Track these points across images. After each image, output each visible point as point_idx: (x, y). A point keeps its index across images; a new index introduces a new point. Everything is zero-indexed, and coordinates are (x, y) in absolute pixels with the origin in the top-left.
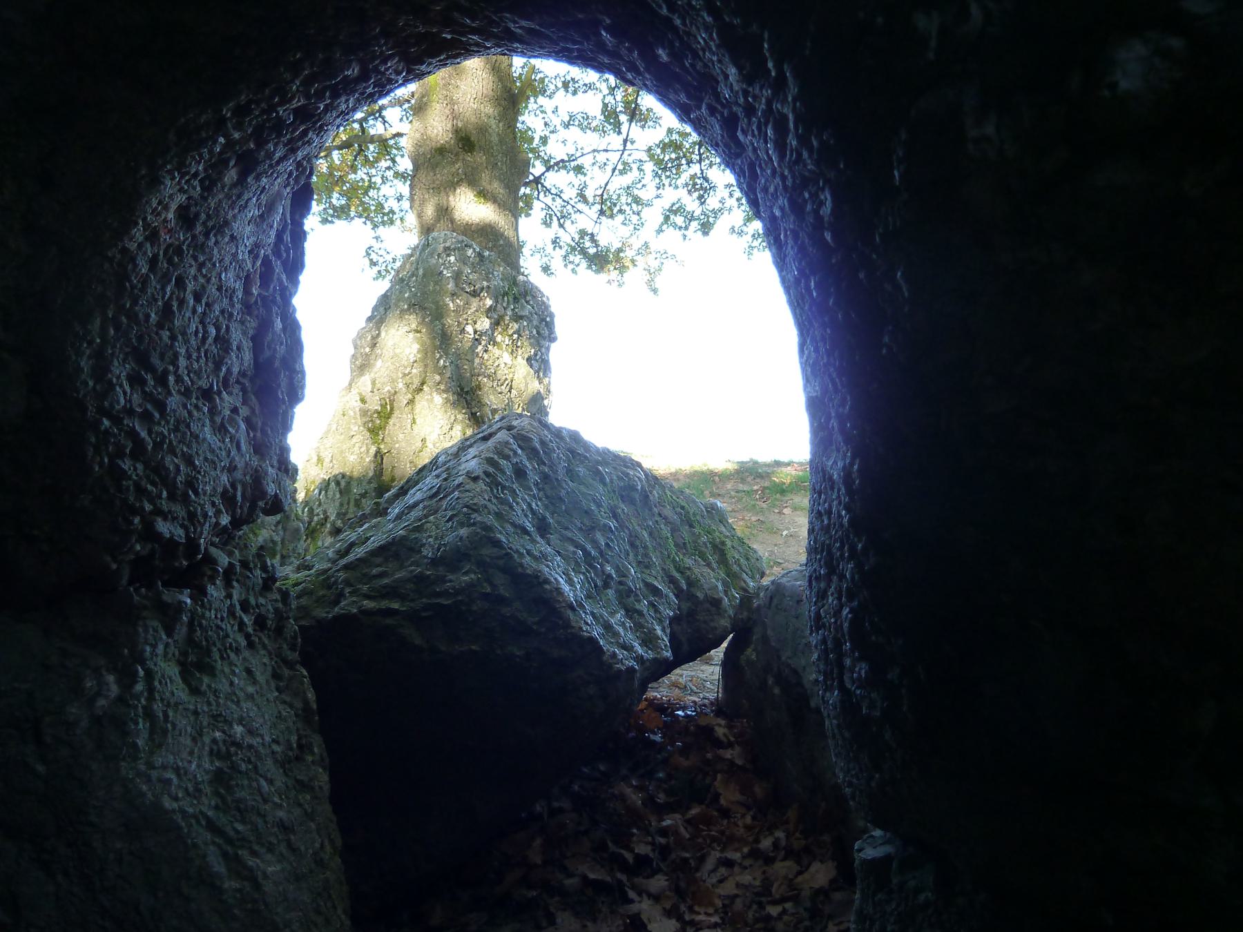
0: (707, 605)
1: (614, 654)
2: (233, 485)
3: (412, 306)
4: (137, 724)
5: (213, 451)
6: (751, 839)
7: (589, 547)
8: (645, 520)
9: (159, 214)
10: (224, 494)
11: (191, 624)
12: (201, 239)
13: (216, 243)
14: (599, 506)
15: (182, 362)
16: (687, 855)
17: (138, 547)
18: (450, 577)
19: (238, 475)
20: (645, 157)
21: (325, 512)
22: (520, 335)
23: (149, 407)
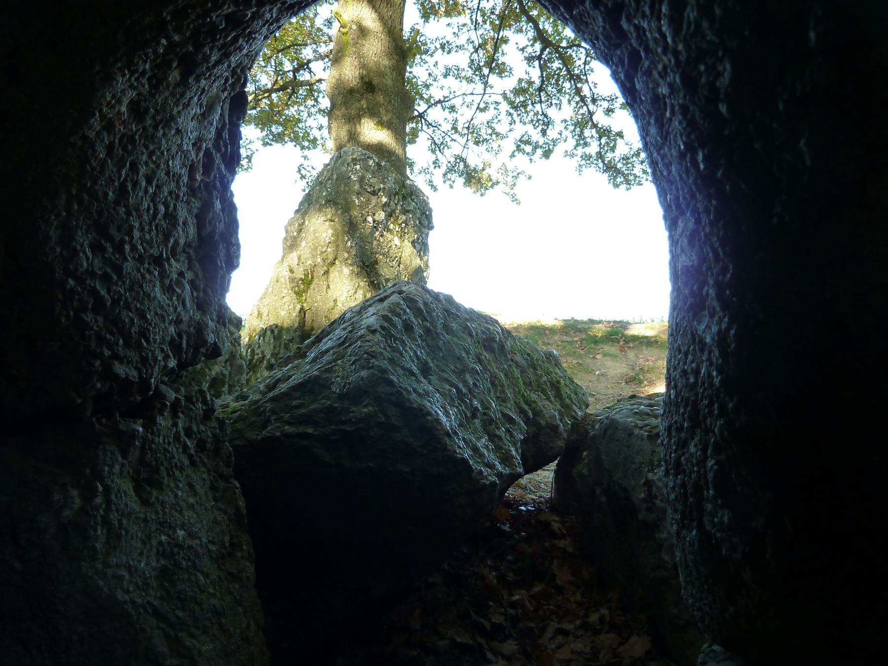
0: (548, 430)
1: (481, 472)
2: (180, 335)
3: (328, 202)
4: (96, 530)
5: (162, 307)
6: (582, 613)
7: (461, 386)
8: (502, 364)
9: (113, 107)
10: (172, 343)
11: (143, 448)
12: (151, 130)
13: (164, 135)
14: (468, 353)
15: (136, 234)
16: (532, 625)
17: (99, 385)
18: (353, 409)
19: (184, 327)
20: (500, 99)
21: (263, 353)
22: (407, 224)
23: (108, 270)
